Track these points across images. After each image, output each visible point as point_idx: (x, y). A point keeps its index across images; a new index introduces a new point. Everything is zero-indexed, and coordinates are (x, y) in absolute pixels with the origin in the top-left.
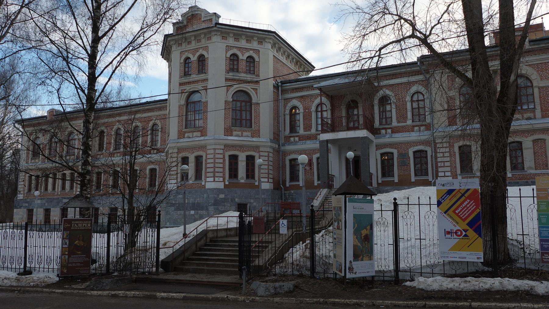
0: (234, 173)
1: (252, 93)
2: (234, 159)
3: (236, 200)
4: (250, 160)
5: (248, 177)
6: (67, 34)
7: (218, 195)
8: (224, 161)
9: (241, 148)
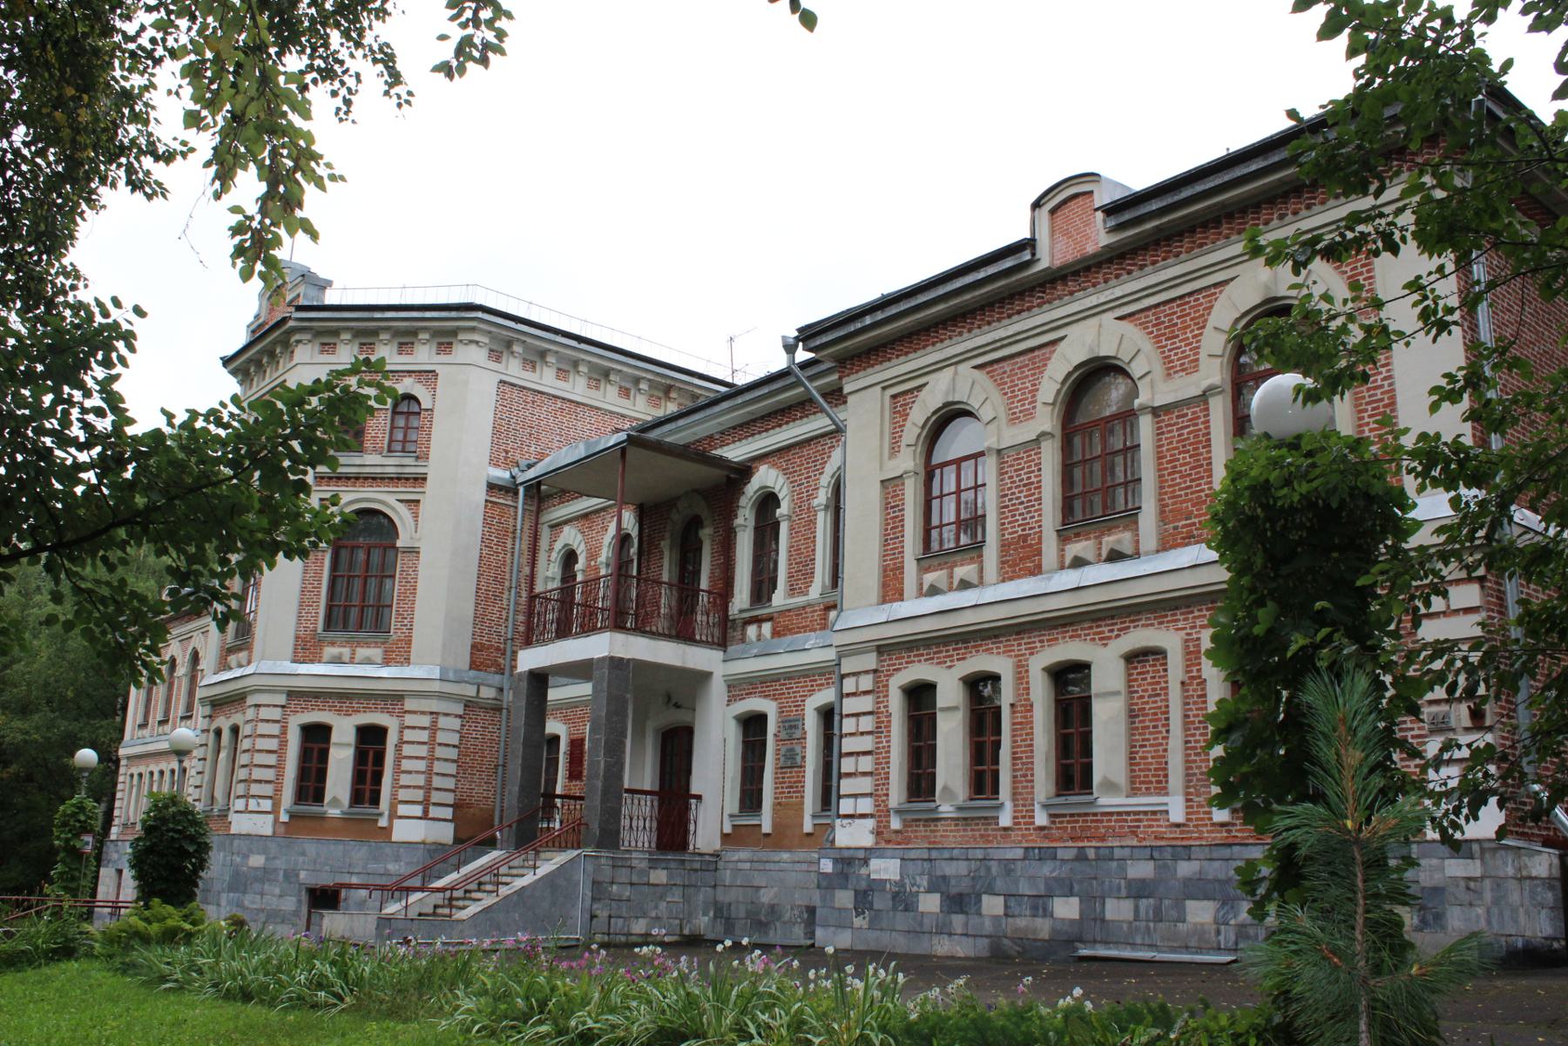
0: (311, 783)
1: (401, 516)
2: (316, 737)
3: (303, 875)
4: (371, 740)
5: (357, 798)
6: (958, 492)
7: (246, 857)
8: (283, 744)
9: (343, 698)
